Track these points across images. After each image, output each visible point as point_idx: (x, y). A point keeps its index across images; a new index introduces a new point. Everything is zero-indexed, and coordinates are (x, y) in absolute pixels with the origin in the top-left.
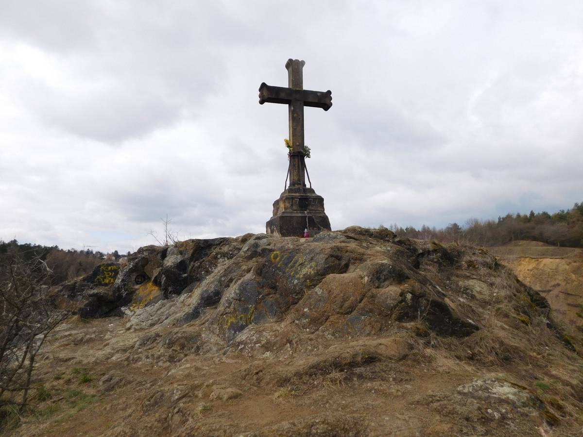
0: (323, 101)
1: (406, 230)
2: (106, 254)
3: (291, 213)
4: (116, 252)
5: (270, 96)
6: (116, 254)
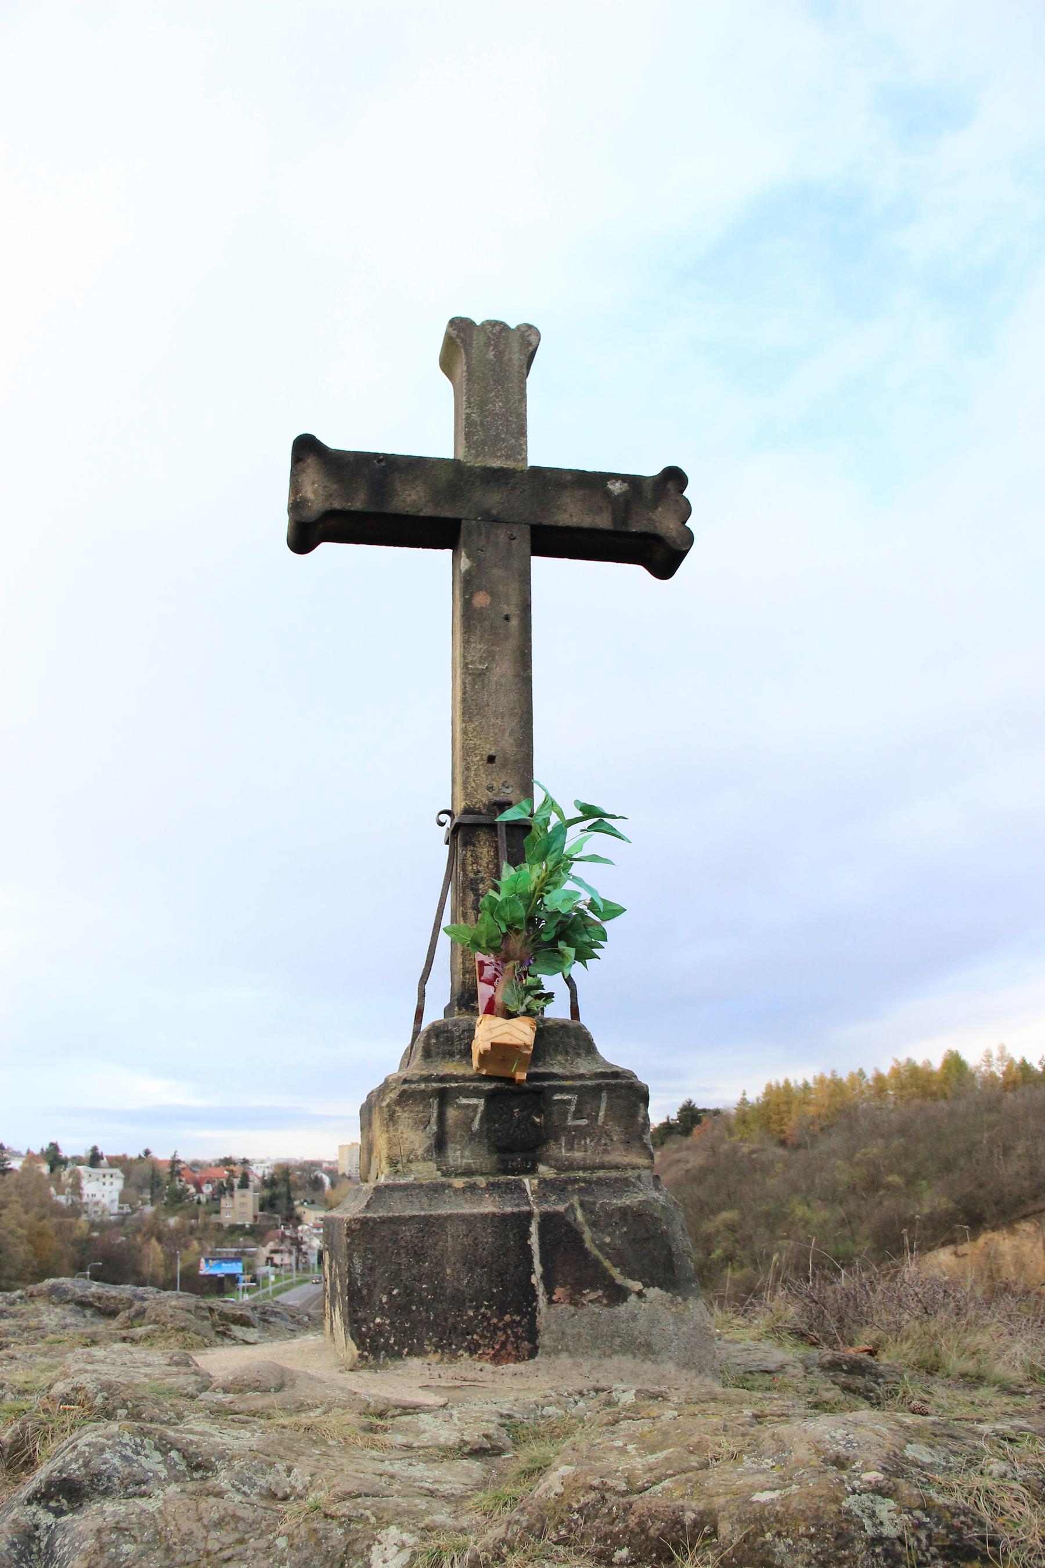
0: (638, 524)
1: (1040, 1063)
2: (24, 1152)
3: (436, 1190)
4: (54, 1147)
5: (337, 505)
6: (53, 1157)
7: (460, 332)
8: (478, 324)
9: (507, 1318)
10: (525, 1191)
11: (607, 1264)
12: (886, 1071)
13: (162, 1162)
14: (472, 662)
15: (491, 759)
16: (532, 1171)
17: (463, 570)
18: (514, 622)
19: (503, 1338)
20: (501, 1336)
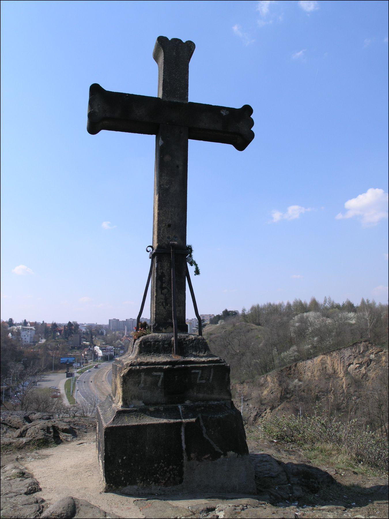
0: (233, 127)
7: (162, 41)
8: (170, 39)
9: (171, 467)
10: (179, 411)
11: (212, 443)
12: (292, 303)
13: (49, 324)
14: (163, 185)
15: (169, 226)
16: (182, 402)
17: (160, 145)
18: (181, 168)
19: (169, 476)
20: (168, 475)
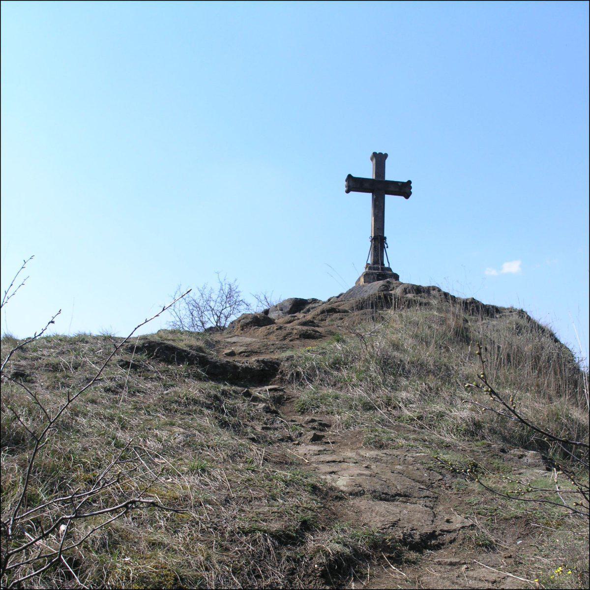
0: (403, 189)
